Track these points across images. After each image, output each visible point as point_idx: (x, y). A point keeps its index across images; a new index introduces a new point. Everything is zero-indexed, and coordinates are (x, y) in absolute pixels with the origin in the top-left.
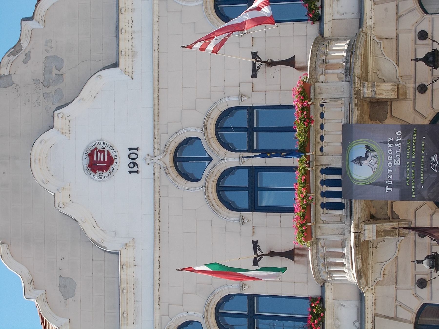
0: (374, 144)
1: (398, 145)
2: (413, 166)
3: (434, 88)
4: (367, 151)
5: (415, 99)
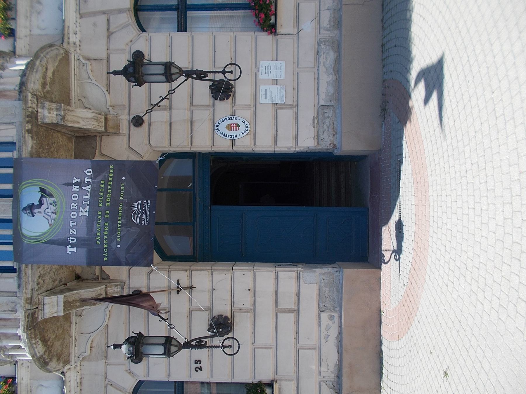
0: (52, 186)
1: (87, 188)
2: (106, 216)
3: (151, 121)
4: (42, 196)
5: (129, 134)
